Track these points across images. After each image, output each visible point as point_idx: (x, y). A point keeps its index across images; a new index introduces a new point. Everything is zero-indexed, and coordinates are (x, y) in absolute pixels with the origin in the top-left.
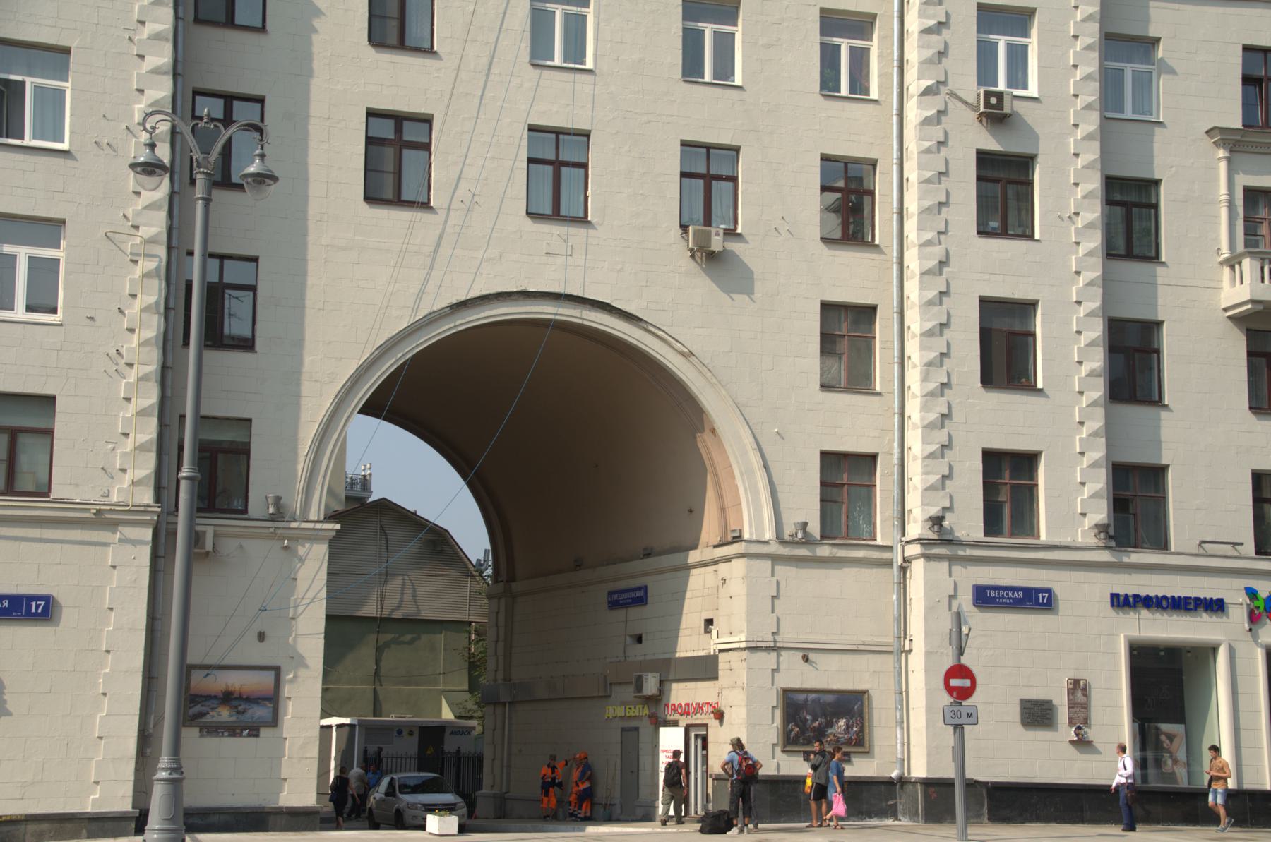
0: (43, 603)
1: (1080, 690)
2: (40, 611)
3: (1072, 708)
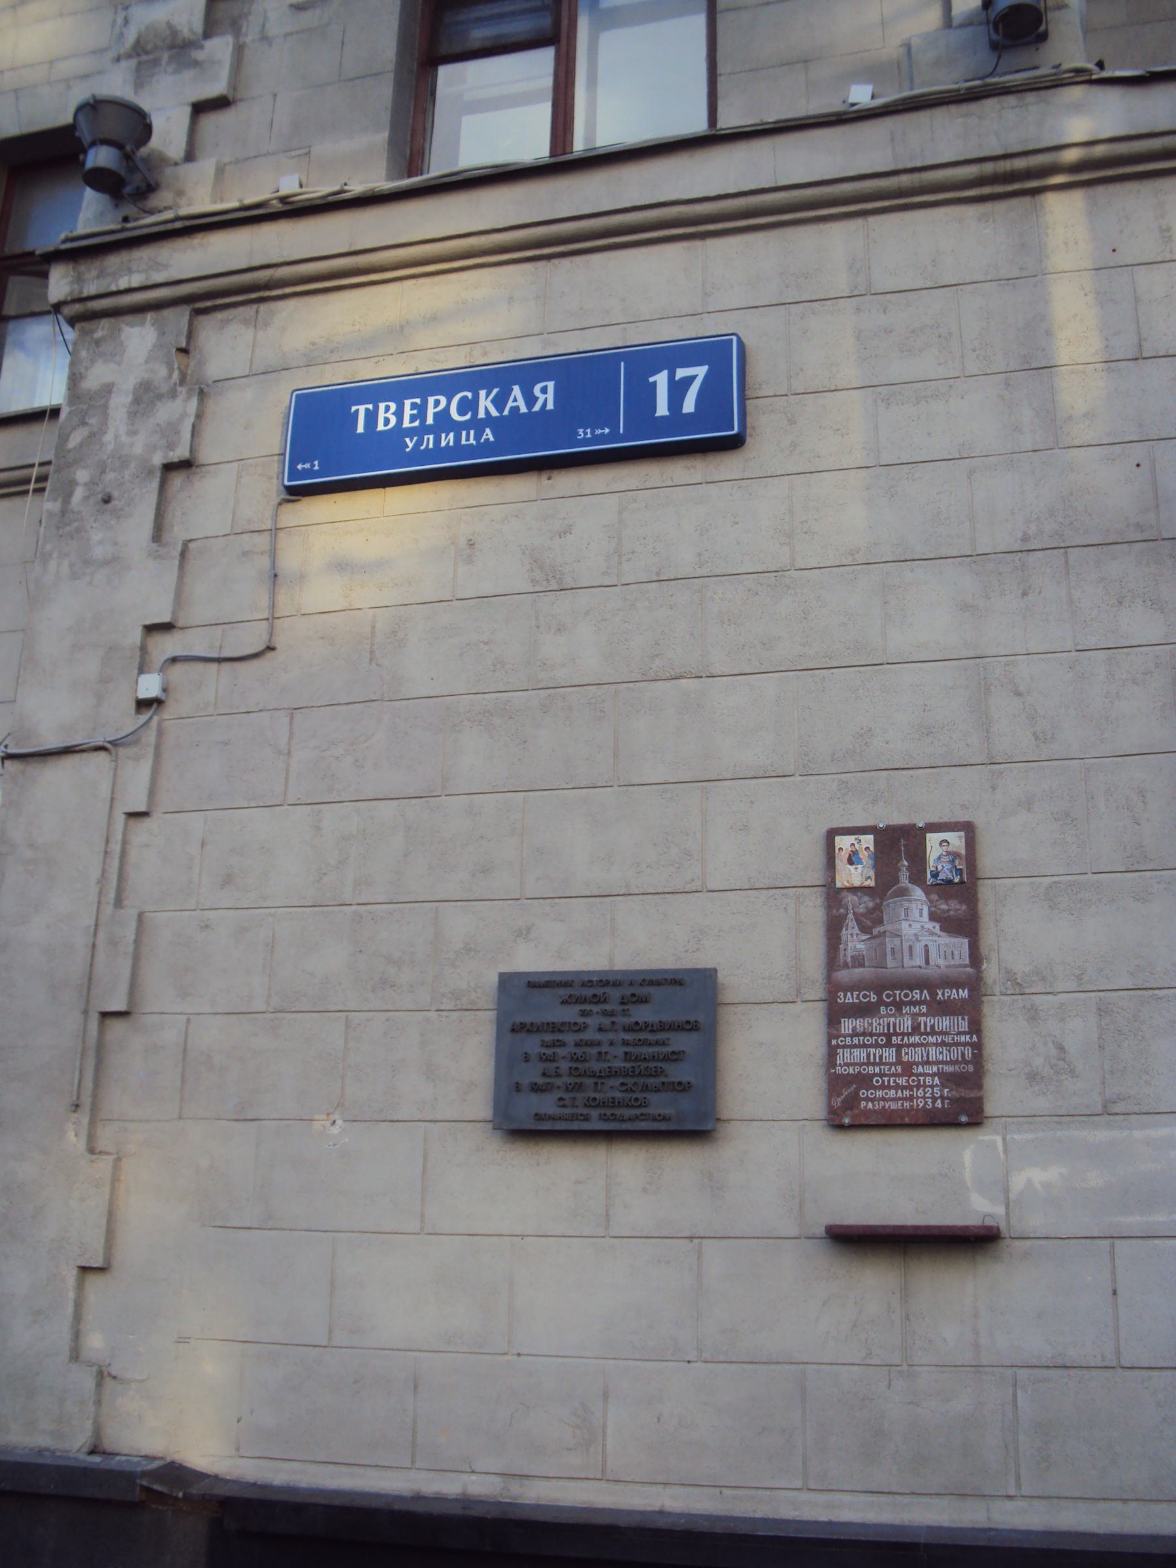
0: (701, 371)
1: (918, 893)
2: (689, 406)
3: (864, 1010)
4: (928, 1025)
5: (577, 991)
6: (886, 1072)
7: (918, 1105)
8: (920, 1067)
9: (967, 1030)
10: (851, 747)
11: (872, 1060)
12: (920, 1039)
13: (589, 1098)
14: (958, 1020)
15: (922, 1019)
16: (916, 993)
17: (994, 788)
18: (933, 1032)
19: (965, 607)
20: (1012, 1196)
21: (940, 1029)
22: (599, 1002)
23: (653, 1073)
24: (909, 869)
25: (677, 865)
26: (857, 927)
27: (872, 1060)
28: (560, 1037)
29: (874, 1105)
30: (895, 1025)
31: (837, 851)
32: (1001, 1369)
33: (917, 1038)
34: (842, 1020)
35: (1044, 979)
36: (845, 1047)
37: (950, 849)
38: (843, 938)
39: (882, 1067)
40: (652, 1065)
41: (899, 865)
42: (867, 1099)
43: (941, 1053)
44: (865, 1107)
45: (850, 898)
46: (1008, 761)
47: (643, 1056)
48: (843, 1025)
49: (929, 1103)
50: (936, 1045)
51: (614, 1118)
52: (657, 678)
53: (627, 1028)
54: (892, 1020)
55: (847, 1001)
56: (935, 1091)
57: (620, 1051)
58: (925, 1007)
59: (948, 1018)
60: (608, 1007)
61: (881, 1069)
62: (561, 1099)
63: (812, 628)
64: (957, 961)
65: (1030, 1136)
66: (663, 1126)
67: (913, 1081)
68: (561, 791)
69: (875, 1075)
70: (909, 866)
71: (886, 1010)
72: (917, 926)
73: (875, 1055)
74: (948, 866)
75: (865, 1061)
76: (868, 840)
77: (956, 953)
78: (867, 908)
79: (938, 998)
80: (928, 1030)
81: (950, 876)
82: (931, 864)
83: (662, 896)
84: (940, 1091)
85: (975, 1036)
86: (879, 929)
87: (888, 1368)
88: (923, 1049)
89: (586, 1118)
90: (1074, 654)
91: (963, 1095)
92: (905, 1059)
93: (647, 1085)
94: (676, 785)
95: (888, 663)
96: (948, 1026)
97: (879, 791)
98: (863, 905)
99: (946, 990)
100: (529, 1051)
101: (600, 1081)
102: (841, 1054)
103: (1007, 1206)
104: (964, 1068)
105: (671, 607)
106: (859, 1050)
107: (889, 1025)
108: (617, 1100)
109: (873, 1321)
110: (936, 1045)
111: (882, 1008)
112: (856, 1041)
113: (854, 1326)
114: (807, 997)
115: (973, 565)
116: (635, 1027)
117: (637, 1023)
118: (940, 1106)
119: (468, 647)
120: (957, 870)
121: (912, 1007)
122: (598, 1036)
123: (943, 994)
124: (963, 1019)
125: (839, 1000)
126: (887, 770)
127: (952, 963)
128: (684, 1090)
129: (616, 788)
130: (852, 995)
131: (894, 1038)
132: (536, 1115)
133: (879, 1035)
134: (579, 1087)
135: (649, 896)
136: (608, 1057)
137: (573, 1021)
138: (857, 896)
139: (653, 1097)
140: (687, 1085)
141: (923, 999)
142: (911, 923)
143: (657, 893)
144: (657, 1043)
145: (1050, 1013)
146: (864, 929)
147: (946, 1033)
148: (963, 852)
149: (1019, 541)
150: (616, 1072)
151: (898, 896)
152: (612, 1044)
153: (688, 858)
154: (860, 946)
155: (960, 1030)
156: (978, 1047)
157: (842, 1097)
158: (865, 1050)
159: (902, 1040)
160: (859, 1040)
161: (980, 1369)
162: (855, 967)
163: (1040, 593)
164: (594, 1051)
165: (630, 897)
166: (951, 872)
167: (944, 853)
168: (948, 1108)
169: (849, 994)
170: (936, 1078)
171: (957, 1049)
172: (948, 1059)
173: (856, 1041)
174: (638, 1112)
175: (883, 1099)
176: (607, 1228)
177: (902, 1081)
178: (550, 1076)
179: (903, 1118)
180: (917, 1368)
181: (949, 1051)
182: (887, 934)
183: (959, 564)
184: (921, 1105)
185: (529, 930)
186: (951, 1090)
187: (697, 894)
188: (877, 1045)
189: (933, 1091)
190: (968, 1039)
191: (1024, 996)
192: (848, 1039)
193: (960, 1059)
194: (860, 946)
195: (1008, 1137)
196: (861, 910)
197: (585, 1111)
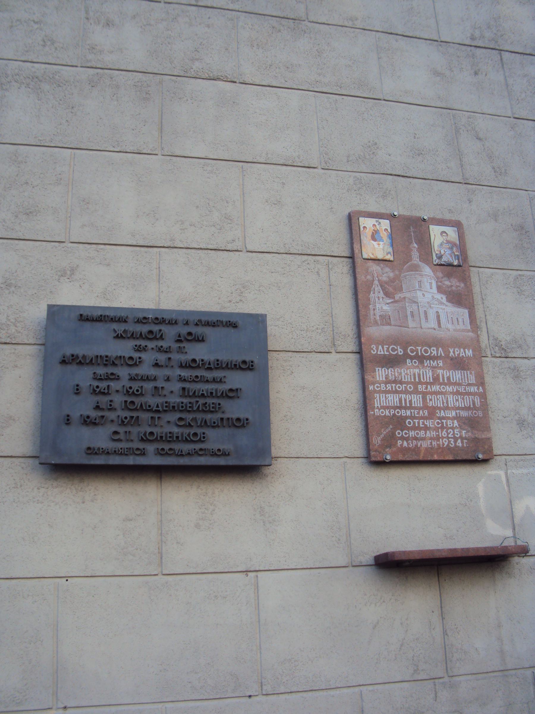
1: (427, 270)
4: (445, 377)
5: (131, 327)
6: (416, 415)
7: (443, 444)
8: (442, 411)
9: (474, 382)
10: (362, 154)
11: (404, 405)
12: (440, 388)
13: (145, 433)
14: (467, 375)
15: (440, 372)
16: (434, 350)
17: (470, 201)
18: (449, 383)
19: (437, 73)
20: (516, 521)
21: (455, 380)
22: (155, 338)
23: (212, 409)
24: (419, 250)
25: (218, 227)
26: (381, 292)
27: (404, 405)
28: (115, 370)
29: (408, 444)
30: (419, 375)
31: (362, 229)
32: (522, 671)
33: (438, 387)
34: (377, 369)
35: (520, 347)
36: (380, 392)
37: (449, 239)
38: (372, 300)
39: (412, 411)
40: (210, 401)
41: (411, 246)
42: (402, 438)
43: (457, 400)
44: (402, 445)
45: (375, 268)
46: (477, 183)
47: (201, 392)
48: (377, 373)
49: (452, 442)
50: (453, 393)
51: (171, 453)
52: (197, 76)
53: (184, 365)
54: (417, 371)
55: (379, 353)
56: (456, 433)
57: (177, 386)
58: (441, 361)
59: (459, 372)
60: (164, 344)
61: (411, 413)
62: (116, 433)
63: (325, 64)
64: (461, 327)
65: (525, 471)
66: (222, 461)
67: (438, 423)
68: (108, 152)
69: (406, 417)
70: (418, 248)
71: (412, 362)
72: (428, 296)
73: (405, 400)
74: (448, 252)
75: (398, 405)
76: (385, 224)
77: (460, 320)
78: (388, 277)
79: (450, 355)
80: (446, 381)
81: (451, 259)
82: (436, 248)
83: (206, 251)
84: (460, 432)
85: (481, 388)
86: (399, 295)
87: (433, 681)
88: (443, 396)
89: (143, 453)
90: (512, 119)
91: (477, 436)
92: (430, 404)
93: (206, 421)
94: (215, 161)
95: (384, 100)
96: (460, 378)
97: (387, 190)
98: (385, 274)
99: (456, 349)
100: (81, 384)
101: (156, 416)
102: (378, 398)
103: (514, 529)
104: (475, 414)
105: (208, 26)
106: (392, 395)
107: (414, 375)
108: (175, 435)
109: (417, 639)
110: (453, 393)
111: (408, 361)
112: (389, 387)
113: (402, 645)
114: (340, 349)
115: (440, 47)
116: (192, 364)
117: (194, 361)
118: (460, 445)
119: (18, 23)
120: (455, 255)
121: (431, 361)
122: (153, 372)
123: (454, 352)
124: (471, 373)
125: (372, 351)
126: (391, 175)
127: (458, 327)
128: (243, 426)
129: (160, 157)
130: (383, 348)
131: (420, 386)
132: (89, 448)
133: (407, 383)
134: (137, 421)
135: (193, 251)
136: (165, 392)
137: (127, 356)
138: (380, 266)
139: (211, 433)
140: (245, 422)
141: (439, 355)
142: (424, 293)
143: (201, 249)
144: (214, 381)
145: (528, 373)
146: (387, 294)
147: (459, 384)
148: (458, 242)
149: (469, 39)
150: (174, 407)
151: (412, 271)
152: (168, 379)
153: (229, 221)
154: (386, 308)
155: (470, 382)
156: (483, 396)
157: (382, 436)
158: (397, 395)
159: (426, 388)
160: (392, 387)
161: (506, 673)
162: (383, 325)
163: (486, 75)
164: (148, 386)
165: (175, 250)
166: (451, 256)
167: (445, 241)
168: (467, 446)
169: (380, 347)
170: (455, 421)
171: (469, 398)
172: (463, 406)
173: (389, 387)
174: (198, 446)
175: (416, 439)
176: (161, 564)
177: (429, 423)
178: (103, 409)
179: (432, 456)
180: (457, 679)
181: (463, 399)
182: (407, 300)
183: (430, 44)
184: (446, 444)
185: (73, 271)
186: (468, 432)
187: (237, 253)
188: (406, 392)
189: (454, 432)
190: (476, 390)
191: (508, 359)
192: (383, 385)
193: (472, 406)
194: (386, 308)
195: (509, 471)
196: (384, 278)
197: (141, 446)
